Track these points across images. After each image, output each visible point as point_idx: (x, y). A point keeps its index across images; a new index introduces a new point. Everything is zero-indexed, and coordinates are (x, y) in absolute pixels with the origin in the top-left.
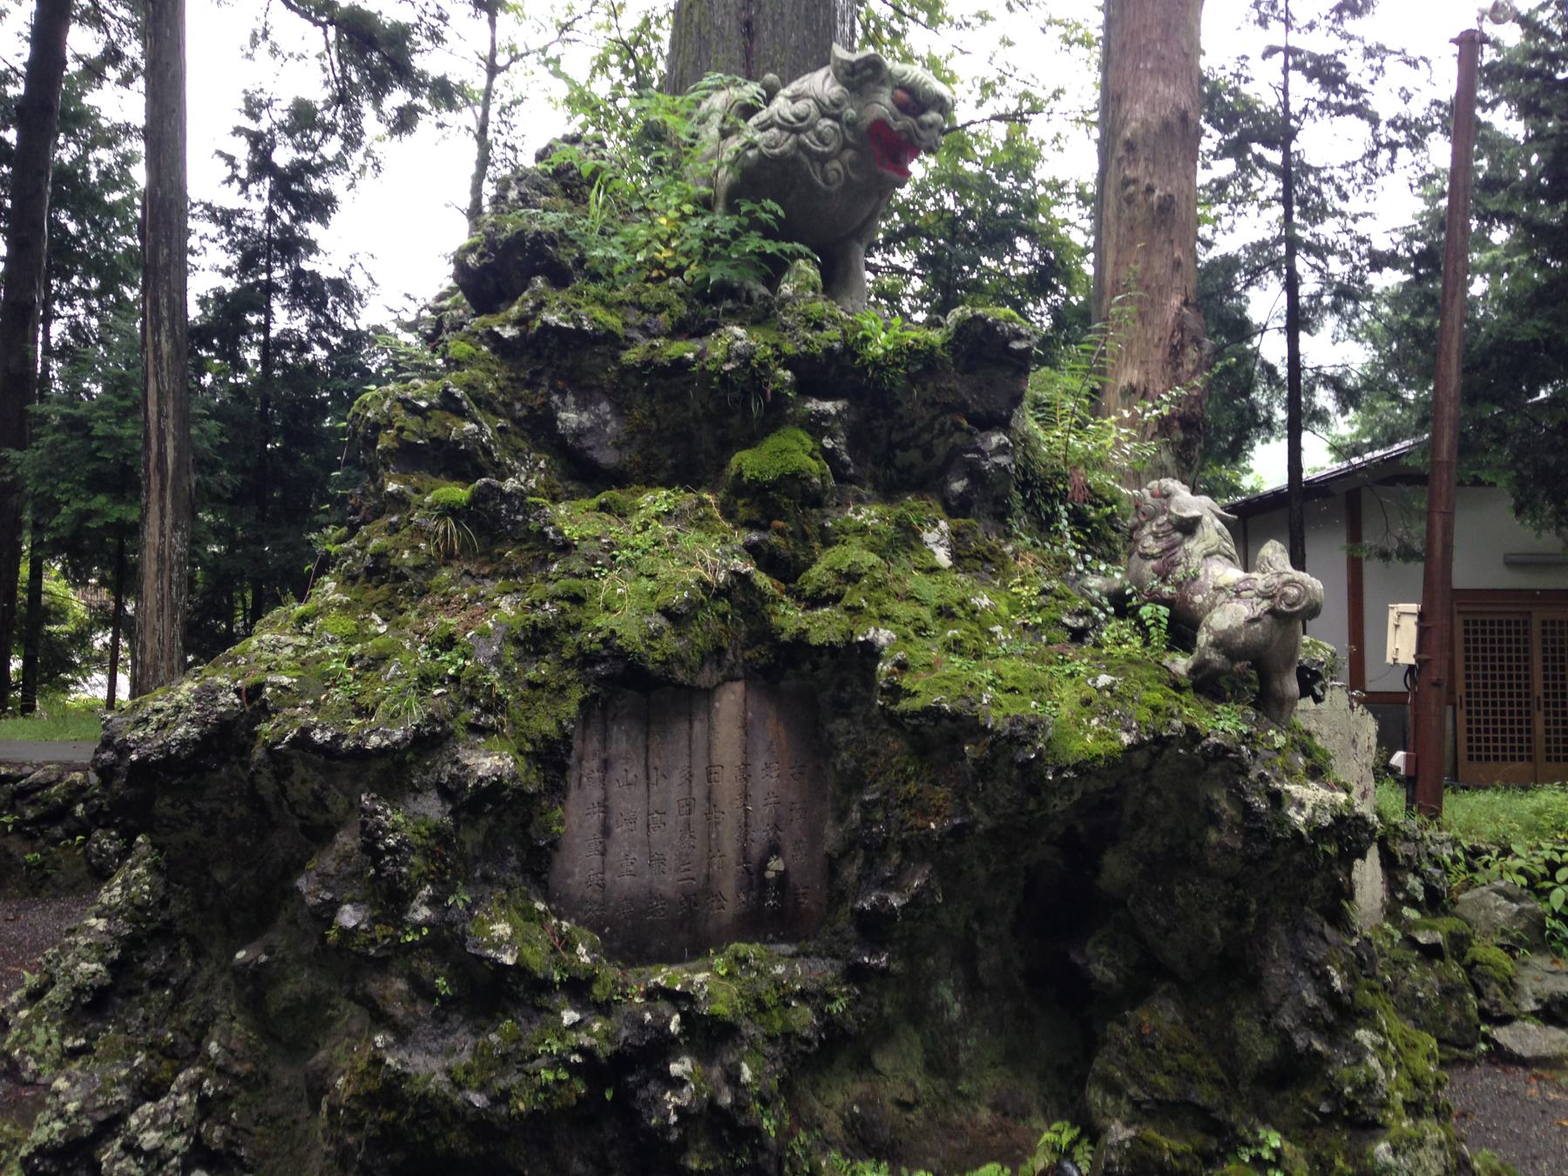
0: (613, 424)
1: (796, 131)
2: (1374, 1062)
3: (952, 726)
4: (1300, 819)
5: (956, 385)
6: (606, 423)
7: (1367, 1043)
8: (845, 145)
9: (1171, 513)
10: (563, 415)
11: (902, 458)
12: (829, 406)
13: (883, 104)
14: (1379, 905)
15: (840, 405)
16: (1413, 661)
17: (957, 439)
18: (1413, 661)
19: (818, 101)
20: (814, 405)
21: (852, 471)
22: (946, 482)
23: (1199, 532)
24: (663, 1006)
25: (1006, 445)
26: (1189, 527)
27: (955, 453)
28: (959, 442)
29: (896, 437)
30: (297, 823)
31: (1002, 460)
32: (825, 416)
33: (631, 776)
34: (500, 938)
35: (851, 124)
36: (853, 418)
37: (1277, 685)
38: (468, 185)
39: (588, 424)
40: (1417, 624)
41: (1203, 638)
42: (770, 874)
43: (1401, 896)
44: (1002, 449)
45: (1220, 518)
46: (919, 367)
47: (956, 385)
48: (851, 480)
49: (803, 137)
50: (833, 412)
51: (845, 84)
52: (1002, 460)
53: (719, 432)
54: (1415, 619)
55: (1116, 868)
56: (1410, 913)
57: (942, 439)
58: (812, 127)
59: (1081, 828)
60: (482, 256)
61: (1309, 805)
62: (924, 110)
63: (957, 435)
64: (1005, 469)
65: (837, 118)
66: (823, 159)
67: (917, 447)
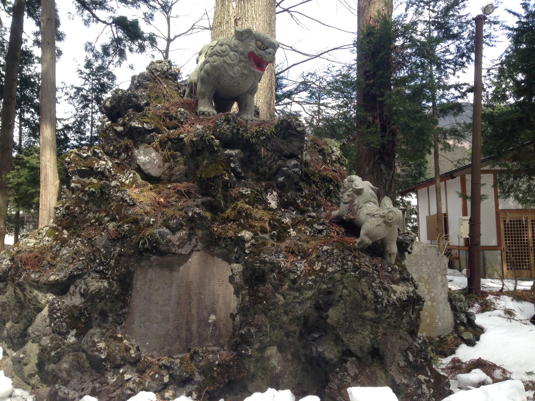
0: (157, 160)
1: (221, 56)
2: (424, 386)
3: (271, 266)
4: (395, 298)
5: (279, 143)
6: (155, 160)
7: (422, 380)
8: (241, 61)
9: (353, 188)
10: (139, 158)
11: (261, 170)
12: (233, 152)
13: (252, 46)
14: (450, 325)
15: (237, 151)
16: (468, 237)
17: (280, 162)
18: (468, 237)
19: (229, 46)
20: (228, 151)
21: (243, 175)
22: (277, 178)
23: (363, 194)
24: (164, 372)
25: (297, 164)
26: (359, 192)
27: (279, 168)
28: (281, 164)
29: (259, 162)
30: (32, 307)
31: (296, 170)
32: (231, 155)
33: (157, 287)
34: (101, 348)
35: (242, 54)
36: (242, 156)
37: (388, 248)
38: (463, 82)
39: (148, 161)
40: (469, 223)
41: (362, 232)
42: (210, 321)
43: (458, 322)
44: (296, 166)
45: (372, 188)
46: (264, 137)
47: (279, 143)
48: (243, 178)
49: (225, 58)
50: (234, 154)
51: (238, 39)
52: (296, 170)
53: (195, 162)
54: (468, 222)
55: (333, 315)
56: (462, 328)
57: (275, 162)
58: (228, 55)
59: (321, 302)
60: (111, 102)
61: (398, 293)
62: (267, 48)
63: (280, 161)
64: (297, 173)
65: (236, 52)
66: (231, 66)
67: (266, 166)
